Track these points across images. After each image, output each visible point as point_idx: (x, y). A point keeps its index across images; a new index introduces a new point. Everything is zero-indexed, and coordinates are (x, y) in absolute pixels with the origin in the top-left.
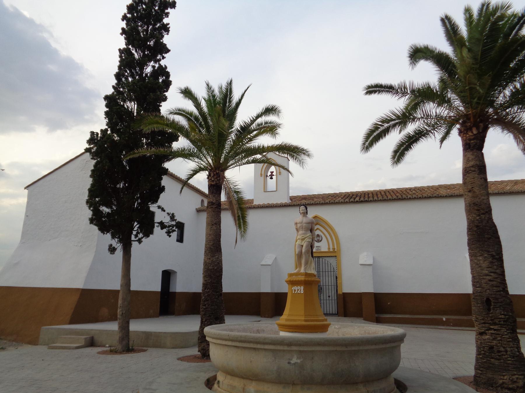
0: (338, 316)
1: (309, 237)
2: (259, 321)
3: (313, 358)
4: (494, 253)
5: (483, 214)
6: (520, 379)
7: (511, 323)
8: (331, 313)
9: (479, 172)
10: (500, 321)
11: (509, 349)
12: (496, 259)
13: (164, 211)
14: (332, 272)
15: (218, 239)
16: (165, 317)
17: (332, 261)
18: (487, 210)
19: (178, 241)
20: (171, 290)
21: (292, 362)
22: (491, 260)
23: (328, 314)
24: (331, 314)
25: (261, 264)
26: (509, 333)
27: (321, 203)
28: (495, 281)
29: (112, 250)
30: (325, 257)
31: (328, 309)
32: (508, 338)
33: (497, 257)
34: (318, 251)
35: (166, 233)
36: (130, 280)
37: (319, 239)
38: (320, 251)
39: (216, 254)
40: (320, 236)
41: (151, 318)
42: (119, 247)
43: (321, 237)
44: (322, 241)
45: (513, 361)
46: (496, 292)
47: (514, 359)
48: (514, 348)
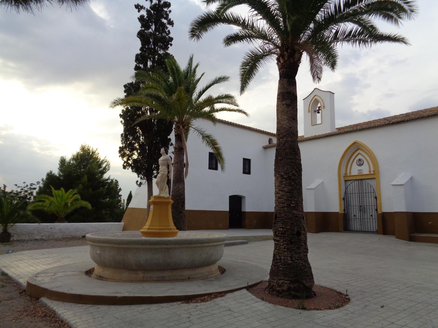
0: (377, 234)
1: (162, 170)
5: (282, 138)
6: (286, 284)
9: (282, 99)
10: (279, 234)
11: (282, 258)
14: (366, 193)
15: (179, 173)
16: (235, 229)
17: (372, 183)
18: (285, 134)
19: (244, 172)
20: (243, 210)
21: (97, 253)
22: (280, 180)
23: (360, 231)
24: (372, 232)
25: (391, 184)
26: (285, 244)
28: (282, 198)
30: (365, 179)
32: (284, 249)
33: (285, 176)
34: (359, 174)
37: (361, 163)
38: (361, 174)
39: (176, 184)
40: (362, 160)
41: (221, 229)
42: (144, 181)
44: (364, 164)
45: (283, 268)
46: (281, 208)
47: (285, 267)
48: (288, 257)
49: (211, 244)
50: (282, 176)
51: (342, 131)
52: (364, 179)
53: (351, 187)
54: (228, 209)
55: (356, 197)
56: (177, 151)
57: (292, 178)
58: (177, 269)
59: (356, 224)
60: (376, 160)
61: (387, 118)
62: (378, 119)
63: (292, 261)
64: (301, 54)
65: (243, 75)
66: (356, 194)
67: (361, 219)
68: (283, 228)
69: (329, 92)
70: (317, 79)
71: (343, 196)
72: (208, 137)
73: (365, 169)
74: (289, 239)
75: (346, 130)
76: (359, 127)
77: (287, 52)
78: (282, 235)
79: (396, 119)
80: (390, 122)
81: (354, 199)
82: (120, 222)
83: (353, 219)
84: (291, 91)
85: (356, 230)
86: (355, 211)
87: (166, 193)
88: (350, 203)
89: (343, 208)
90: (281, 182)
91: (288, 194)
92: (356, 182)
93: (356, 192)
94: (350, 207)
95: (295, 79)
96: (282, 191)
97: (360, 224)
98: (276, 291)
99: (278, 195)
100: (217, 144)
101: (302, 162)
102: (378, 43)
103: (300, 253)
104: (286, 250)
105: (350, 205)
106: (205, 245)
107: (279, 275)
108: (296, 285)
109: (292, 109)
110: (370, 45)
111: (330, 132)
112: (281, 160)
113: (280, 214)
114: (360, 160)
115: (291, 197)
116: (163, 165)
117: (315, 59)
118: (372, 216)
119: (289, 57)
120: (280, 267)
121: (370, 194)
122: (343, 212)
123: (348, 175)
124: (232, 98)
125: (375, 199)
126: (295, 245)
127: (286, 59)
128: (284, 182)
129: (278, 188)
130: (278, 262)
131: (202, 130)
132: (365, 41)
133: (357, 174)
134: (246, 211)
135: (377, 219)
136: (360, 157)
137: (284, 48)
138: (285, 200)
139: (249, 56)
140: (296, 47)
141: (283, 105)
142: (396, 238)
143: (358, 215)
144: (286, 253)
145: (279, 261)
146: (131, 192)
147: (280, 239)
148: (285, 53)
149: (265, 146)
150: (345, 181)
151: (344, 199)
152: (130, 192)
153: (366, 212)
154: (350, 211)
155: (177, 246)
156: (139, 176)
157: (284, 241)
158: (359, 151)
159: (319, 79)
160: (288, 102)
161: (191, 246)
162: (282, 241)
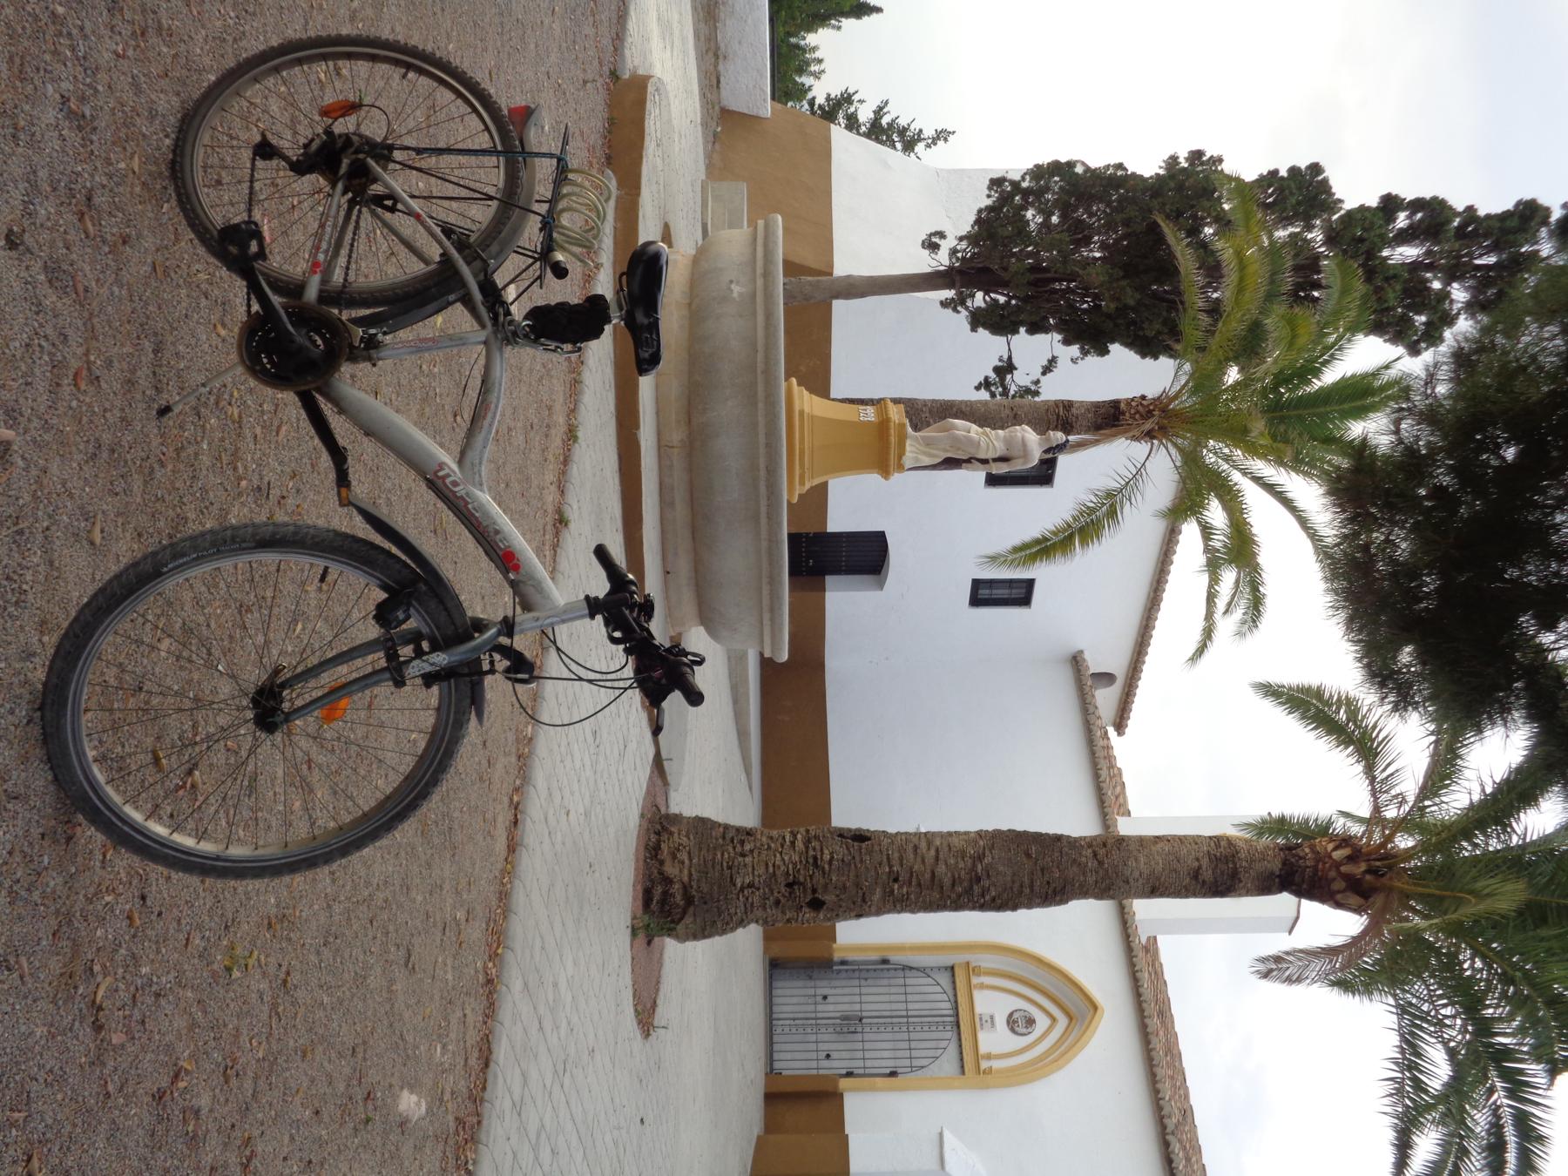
0: (766, 1074)
2: (750, 788)
3: (741, 316)
4: (988, 860)
5: (1095, 855)
6: (681, 871)
7: (811, 877)
8: (776, 1056)
10: (814, 849)
11: (748, 860)
12: (974, 865)
13: (1044, 373)
17: (948, 1064)
21: (733, 286)
27: (1147, 1021)
29: (931, 245)
30: (960, 1040)
31: (789, 1056)
33: (979, 867)
34: (977, 1020)
35: (986, 378)
36: (862, 295)
42: (943, 259)
43: (1024, 1031)
49: (767, 622)
50: (981, 857)
51: (1141, 960)
52: (959, 1034)
53: (931, 989)
54: (834, 526)
55: (894, 1006)
56: (1058, 415)
57: (975, 887)
58: (694, 538)
59: (795, 1000)
60: (1032, 1080)
61: (1189, 1120)
62: (1187, 1088)
63: (742, 889)
64: (1358, 910)
65: (1318, 693)
66: (903, 1006)
67: (816, 1019)
68: (830, 862)
69: (1295, 915)
70: (1262, 967)
71: (894, 958)
72: (1112, 513)
73: (995, 1041)
74: (802, 879)
75: (1145, 977)
76: (1154, 1023)
77: (1368, 871)
78: (811, 861)
79: (1181, 1154)
80: (1173, 1133)
81: (886, 998)
82: (773, 98)
83: (811, 991)
84: (1240, 881)
85: (776, 1000)
86: (841, 998)
87: (917, 460)
88: (870, 982)
89: (850, 957)
90: (962, 854)
91: (928, 876)
92: (948, 1005)
93: (911, 1006)
94: (856, 982)
95: (1280, 892)
96: (937, 858)
97: (796, 1016)
98: (659, 841)
99: (923, 845)
100: (1084, 543)
101: (1022, 913)
102: (1391, 1135)
103: (765, 909)
104: (771, 870)
105: (863, 982)
106: (767, 616)
107: (700, 849)
108: (678, 898)
109: (1185, 887)
110: (1389, 1110)
111: (1137, 917)
112: (1028, 855)
113: (870, 852)
114: (1030, 1022)
115: (919, 885)
116: (1008, 442)
117: (1331, 961)
118: (828, 1056)
119: (1348, 878)
120: (723, 855)
121: (907, 1054)
122: (837, 956)
123: (975, 980)
124: (1254, 621)
125: (888, 1071)
126: (784, 896)
127: (1343, 869)
128: (961, 865)
129: (945, 844)
130: (734, 848)
131: (1139, 497)
132: (1399, 1092)
133: (978, 1010)
134: (828, 595)
135: (818, 1075)
136: (1042, 1022)
137: (1378, 863)
138: (911, 868)
139: (1375, 727)
140: (1378, 900)
141: (1198, 860)
142: (759, 1138)
143: (830, 1009)
144: (761, 870)
145: (739, 849)
146: (878, 10)
147: (801, 854)
148: (1363, 867)
149: (1084, 660)
150: (952, 968)
151: (885, 961)
152: (878, 5)
153: (841, 1037)
154: (844, 983)
155: (764, 544)
156: (961, 239)
157: (795, 864)
158: (1063, 1021)
159: (1266, 975)
160: (1207, 874)
161: (765, 580)
162: (796, 858)
